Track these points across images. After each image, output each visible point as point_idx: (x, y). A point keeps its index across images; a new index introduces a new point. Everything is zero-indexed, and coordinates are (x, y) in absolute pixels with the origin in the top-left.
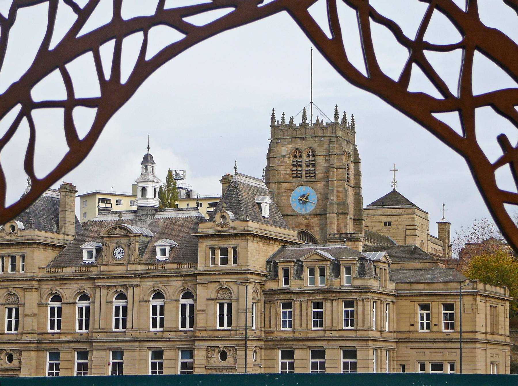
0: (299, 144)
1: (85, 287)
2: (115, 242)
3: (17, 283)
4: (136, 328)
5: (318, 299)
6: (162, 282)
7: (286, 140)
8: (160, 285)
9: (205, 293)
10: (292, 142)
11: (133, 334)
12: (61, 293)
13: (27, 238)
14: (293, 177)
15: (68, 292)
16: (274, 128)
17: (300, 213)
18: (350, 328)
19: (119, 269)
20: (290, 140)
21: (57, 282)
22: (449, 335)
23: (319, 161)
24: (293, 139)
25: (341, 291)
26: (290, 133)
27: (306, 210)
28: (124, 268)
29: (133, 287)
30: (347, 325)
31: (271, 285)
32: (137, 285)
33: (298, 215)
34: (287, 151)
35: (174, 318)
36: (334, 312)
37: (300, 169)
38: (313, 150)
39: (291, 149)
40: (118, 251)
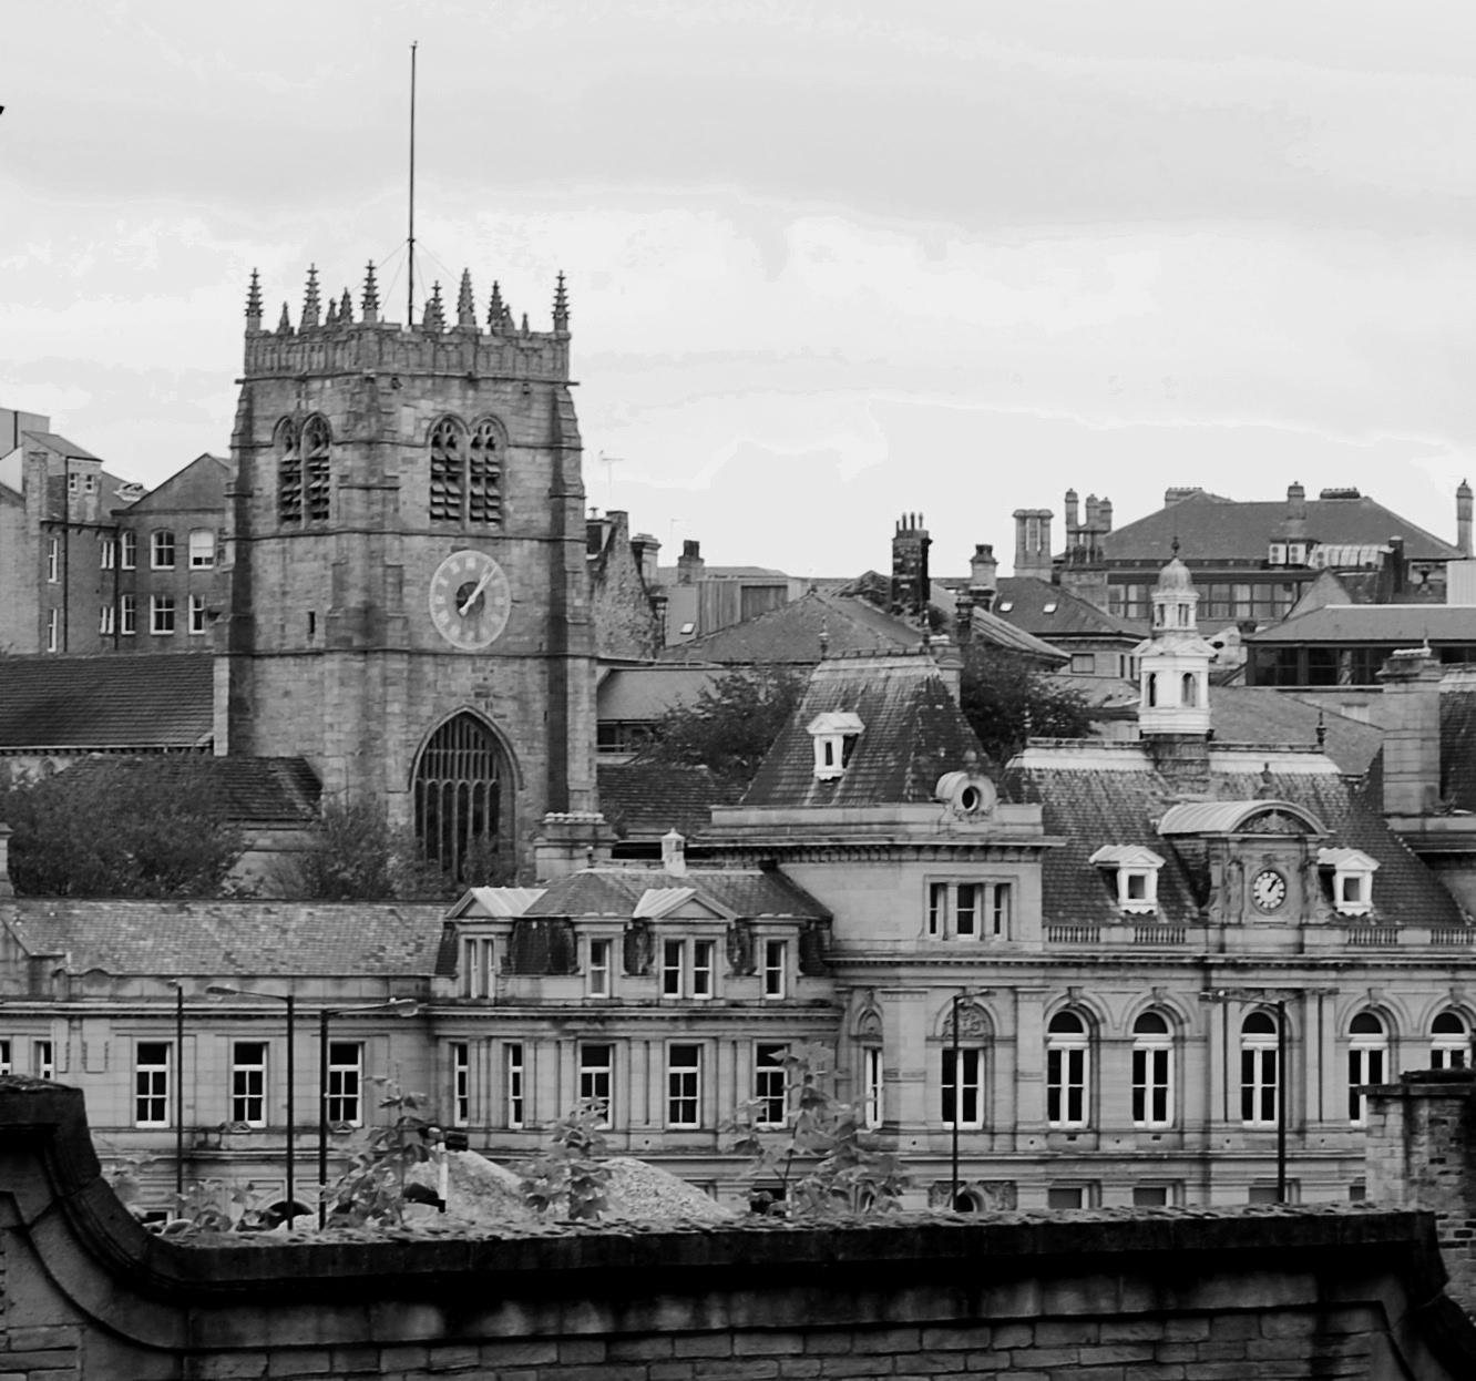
0: (454, 402)
1: (1168, 992)
2: (1259, 855)
3: (992, 972)
4: (1329, 1121)
6: (1393, 984)
7: (418, 382)
8: (1386, 993)
10: (435, 392)
11: (1328, 1137)
12: (1097, 1007)
13: (1019, 829)
14: (433, 517)
15: (1117, 1004)
17: (458, 645)
18: (149, 1124)
20: (429, 383)
21: (1086, 973)
22: (1073, 1139)
23: (516, 467)
24: (439, 381)
26: (428, 359)
27: (477, 639)
28: (1290, 936)
29: (1321, 996)
30: (142, 1116)
32: (1333, 992)
33: (453, 655)
34: (419, 420)
37: (454, 489)
38: (493, 420)
39: (432, 415)
40: (1268, 883)
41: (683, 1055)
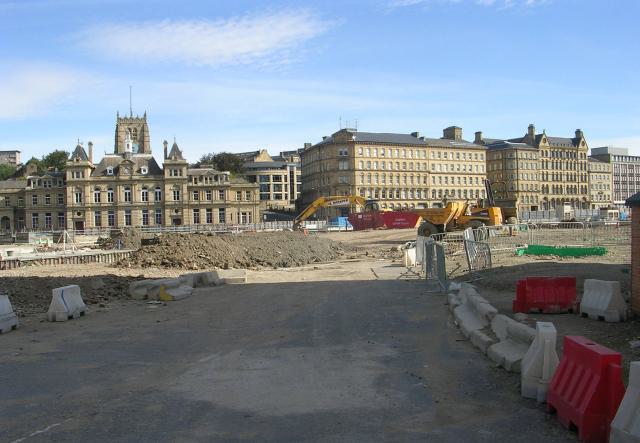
5: (209, 190)
9: (169, 188)
16: (119, 119)
19: (127, 178)
25: (219, 186)
31: (190, 184)
35: (151, 197)
36: (216, 194)
41: (34, 215)
